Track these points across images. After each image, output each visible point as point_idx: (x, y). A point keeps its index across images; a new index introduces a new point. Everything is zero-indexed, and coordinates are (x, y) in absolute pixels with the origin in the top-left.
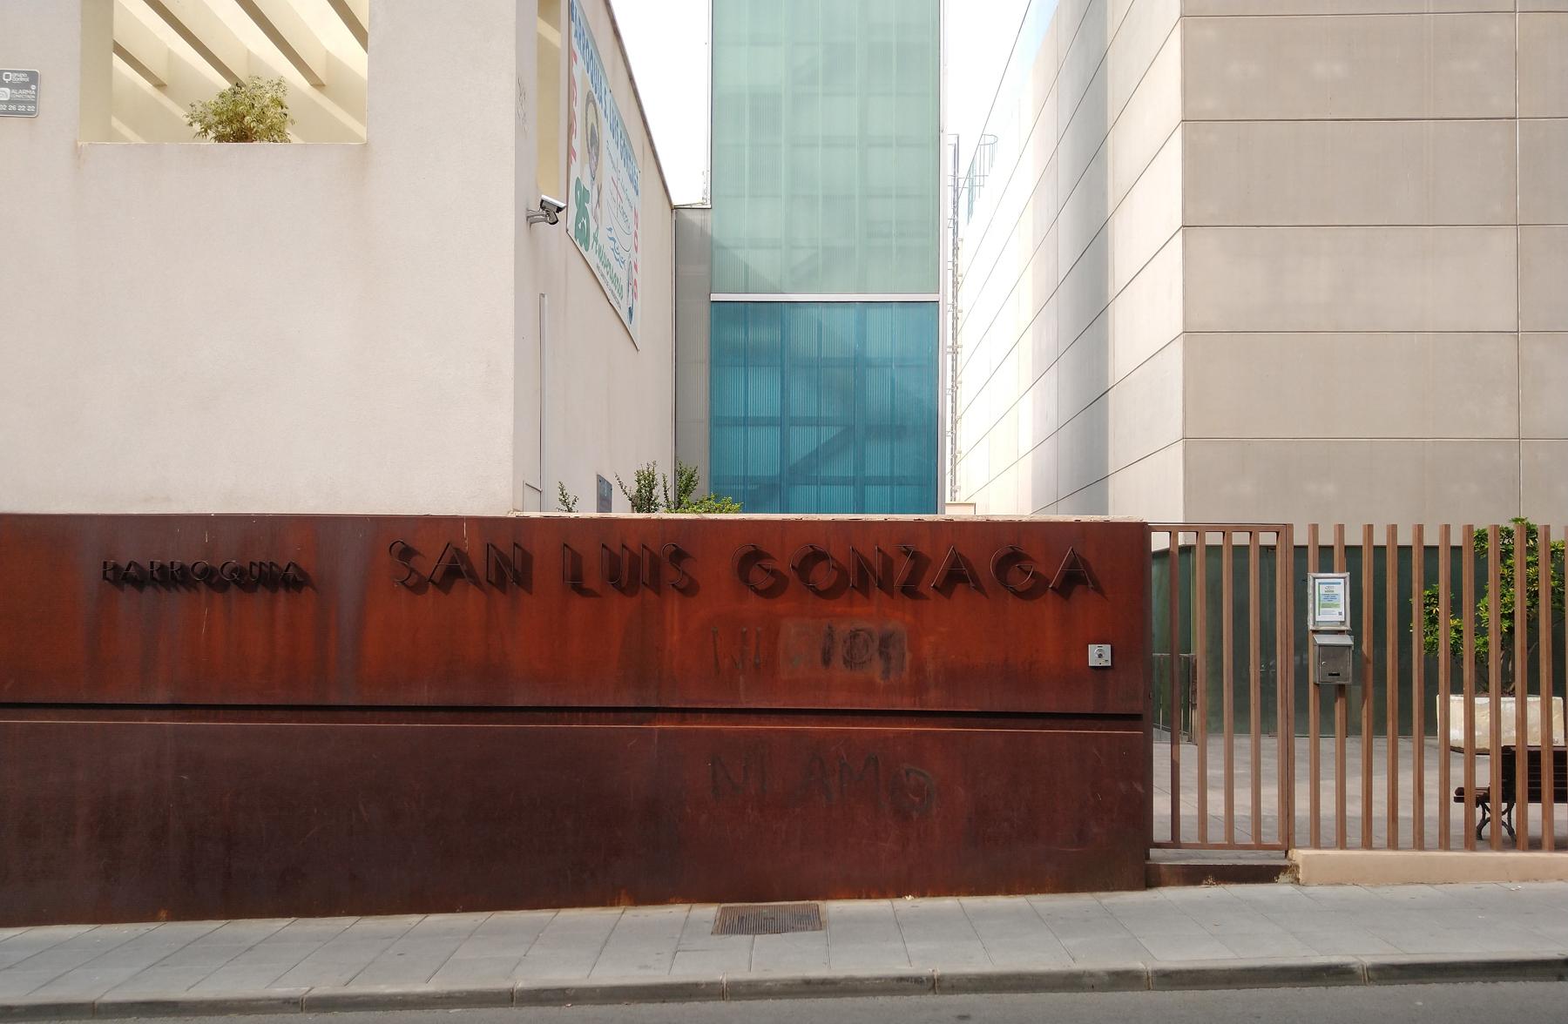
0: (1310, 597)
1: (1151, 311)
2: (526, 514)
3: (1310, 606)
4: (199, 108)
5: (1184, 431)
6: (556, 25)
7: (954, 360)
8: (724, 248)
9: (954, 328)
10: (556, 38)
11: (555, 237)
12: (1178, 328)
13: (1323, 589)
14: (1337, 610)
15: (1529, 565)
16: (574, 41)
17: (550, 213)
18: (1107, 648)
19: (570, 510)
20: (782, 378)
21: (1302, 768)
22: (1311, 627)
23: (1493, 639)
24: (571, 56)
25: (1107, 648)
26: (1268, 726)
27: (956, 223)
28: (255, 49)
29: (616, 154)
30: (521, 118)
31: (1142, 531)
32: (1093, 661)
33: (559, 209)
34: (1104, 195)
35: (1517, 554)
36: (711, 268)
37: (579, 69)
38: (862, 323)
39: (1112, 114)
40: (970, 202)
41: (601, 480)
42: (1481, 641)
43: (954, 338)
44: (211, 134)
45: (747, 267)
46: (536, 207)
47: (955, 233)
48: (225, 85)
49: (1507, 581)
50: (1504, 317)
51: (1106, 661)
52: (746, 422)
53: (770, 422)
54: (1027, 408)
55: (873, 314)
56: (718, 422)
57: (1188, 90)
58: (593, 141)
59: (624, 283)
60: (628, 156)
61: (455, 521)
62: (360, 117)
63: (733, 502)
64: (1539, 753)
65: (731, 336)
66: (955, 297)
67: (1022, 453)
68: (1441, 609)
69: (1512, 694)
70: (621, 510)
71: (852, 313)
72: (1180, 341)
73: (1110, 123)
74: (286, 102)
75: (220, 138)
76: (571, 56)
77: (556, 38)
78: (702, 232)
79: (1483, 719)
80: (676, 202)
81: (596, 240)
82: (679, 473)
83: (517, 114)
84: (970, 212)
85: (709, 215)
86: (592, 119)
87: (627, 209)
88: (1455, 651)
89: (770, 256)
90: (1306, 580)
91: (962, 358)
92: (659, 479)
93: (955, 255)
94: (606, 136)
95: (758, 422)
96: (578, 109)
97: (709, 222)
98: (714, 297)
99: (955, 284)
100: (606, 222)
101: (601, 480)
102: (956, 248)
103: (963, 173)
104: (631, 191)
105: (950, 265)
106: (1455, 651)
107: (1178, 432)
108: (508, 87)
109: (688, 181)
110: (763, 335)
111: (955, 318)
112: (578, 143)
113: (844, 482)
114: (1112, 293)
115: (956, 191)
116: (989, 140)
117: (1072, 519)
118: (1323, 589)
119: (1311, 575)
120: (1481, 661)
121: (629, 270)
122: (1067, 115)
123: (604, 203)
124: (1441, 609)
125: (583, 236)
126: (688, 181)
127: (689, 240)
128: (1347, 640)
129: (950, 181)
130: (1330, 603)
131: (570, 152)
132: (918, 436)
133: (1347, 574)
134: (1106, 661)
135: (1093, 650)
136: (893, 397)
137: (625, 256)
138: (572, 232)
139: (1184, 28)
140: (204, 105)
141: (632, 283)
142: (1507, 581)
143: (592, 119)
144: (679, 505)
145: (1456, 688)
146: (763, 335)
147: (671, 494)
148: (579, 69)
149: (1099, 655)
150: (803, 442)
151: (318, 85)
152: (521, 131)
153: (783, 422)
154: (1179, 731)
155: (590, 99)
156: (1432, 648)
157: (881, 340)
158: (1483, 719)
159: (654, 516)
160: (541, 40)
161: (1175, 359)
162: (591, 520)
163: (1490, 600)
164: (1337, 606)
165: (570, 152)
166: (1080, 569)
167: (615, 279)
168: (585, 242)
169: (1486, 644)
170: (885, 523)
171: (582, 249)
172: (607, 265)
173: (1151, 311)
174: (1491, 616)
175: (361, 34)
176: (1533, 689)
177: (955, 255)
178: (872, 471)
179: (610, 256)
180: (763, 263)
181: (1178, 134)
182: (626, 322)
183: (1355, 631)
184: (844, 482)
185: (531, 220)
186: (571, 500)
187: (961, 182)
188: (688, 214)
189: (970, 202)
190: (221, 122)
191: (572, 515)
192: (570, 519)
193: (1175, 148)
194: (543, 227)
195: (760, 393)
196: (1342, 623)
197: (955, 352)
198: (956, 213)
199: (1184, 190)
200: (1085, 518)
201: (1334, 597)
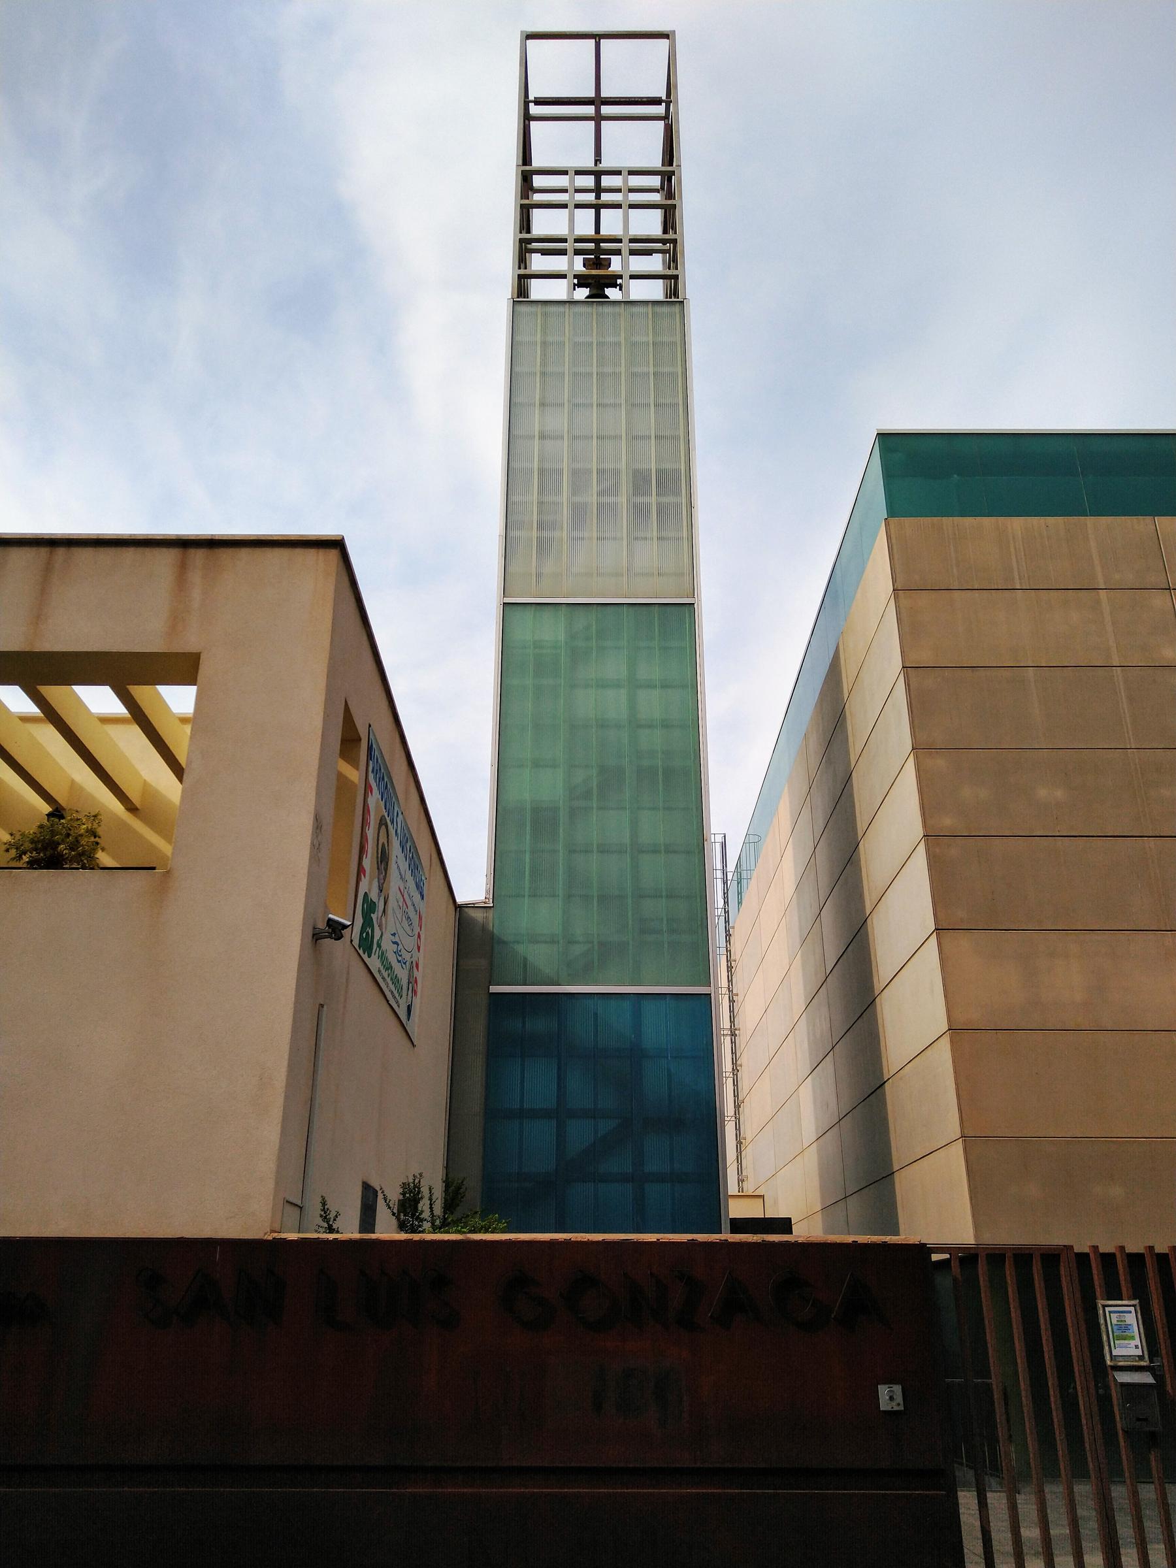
0: (1103, 1327)
1: (915, 1010)
2: (283, 1236)
3: (1105, 1338)
4: (18, 837)
6: (354, 763)
7: (733, 1042)
8: (504, 943)
9: (731, 1011)
10: (354, 775)
11: (340, 951)
13: (1114, 1318)
14: (1133, 1343)
16: (371, 776)
17: (336, 930)
18: (897, 1389)
19: (331, 1230)
20: (559, 1068)
21: (1125, 1531)
24: (368, 788)
25: (897, 1389)
26: (1079, 1472)
27: (727, 912)
28: (78, 778)
29: (404, 865)
30: (316, 848)
31: (922, 1250)
32: (885, 1404)
33: (345, 927)
34: (861, 896)
36: (491, 964)
37: (374, 799)
38: (637, 1015)
39: (861, 826)
40: (740, 893)
41: (366, 1187)
43: (732, 1022)
44: (25, 858)
45: (525, 959)
46: (322, 925)
47: (727, 921)
48: (46, 808)
51: (897, 1405)
52: (523, 1114)
53: (545, 1114)
54: (806, 1093)
55: (648, 1007)
56: (493, 1114)
58: (383, 858)
59: (404, 982)
60: (415, 865)
61: (209, 1244)
62: (168, 838)
63: (499, 1221)
65: (507, 1024)
66: (730, 981)
67: (806, 1145)
70: (387, 1230)
71: (627, 1004)
72: (946, 1038)
73: (860, 834)
74: (100, 831)
75: (33, 865)
76: (368, 788)
77: (354, 775)
78: (484, 928)
80: (460, 899)
81: (379, 946)
82: (447, 1183)
83: (313, 844)
84: (740, 903)
85: (491, 914)
86: (383, 839)
87: (412, 914)
89: (550, 953)
90: (1095, 1308)
91: (741, 1040)
92: (425, 1191)
93: (728, 941)
94: (396, 851)
95: (534, 1114)
96: (371, 833)
97: (492, 921)
98: (494, 989)
99: (730, 968)
100: (391, 929)
101: (366, 1187)
102: (728, 935)
103: (731, 867)
104: (417, 896)
105: (723, 951)
107: (951, 1125)
108: (305, 822)
109: (471, 882)
110: (540, 1025)
111: (732, 1001)
112: (367, 863)
114: (879, 983)
115: (725, 882)
116: (752, 839)
117: (849, 1239)
119: (1100, 1303)
121: (411, 969)
122: (821, 823)
123: (389, 911)
125: (367, 944)
126: (471, 882)
127: (472, 936)
128: (1147, 1378)
129: (719, 874)
131: (361, 870)
132: (693, 1125)
133: (1136, 1302)
134: (897, 1405)
135: (883, 1391)
137: (407, 956)
138: (356, 943)
139: (917, 758)
140: (23, 835)
141: (413, 981)
143: (383, 839)
144: (444, 1226)
146: (540, 1025)
147: (438, 1210)
148: (374, 799)
149: (889, 1397)
150: (580, 1134)
151: (132, 808)
152: (315, 858)
153: (560, 1114)
154: (987, 1469)
155: (382, 823)
157: (657, 1031)
159: (416, 1237)
160: (340, 777)
161: (943, 1054)
162: (351, 1242)
164: (1133, 1338)
165: (361, 870)
166: (859, 1292)
167: (396, 980)
168: (369, 950)
170: (658, 1243)
171: (365, 957)
172: (389, 967)
175: (178, 770)
177: (728, 941)
179: (392, 958)
180: (540, 956)
181: (922, 848)
182: (403, 1017)
185: (317, 936)
186: (332, 1215)
187: (730, 877)
188: (395, 1211)
189: (740, 893)
190: (36, 849)
191: (331, 1237)
192: (327, 1241)
193: (920, 860)
194: (327, 942)
195: (536, 1083)
196: (1141, 1358)
197: (733, 1035)
198: (726, 902)
200: (863, 1239)
201: (1127, 1327)
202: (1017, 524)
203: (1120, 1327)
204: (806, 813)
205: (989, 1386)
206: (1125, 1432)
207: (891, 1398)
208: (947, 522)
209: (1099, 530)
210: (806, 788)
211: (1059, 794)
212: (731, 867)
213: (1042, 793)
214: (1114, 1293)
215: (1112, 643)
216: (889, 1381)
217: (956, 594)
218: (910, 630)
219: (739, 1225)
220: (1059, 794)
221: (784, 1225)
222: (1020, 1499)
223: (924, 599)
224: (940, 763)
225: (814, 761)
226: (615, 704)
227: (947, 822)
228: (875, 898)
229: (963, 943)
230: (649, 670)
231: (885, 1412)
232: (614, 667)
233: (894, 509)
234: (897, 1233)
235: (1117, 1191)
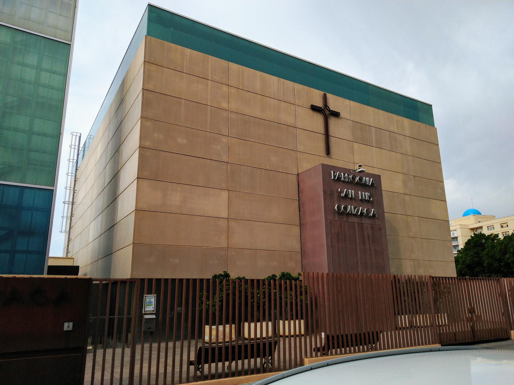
1: (127, 203)
5: (133, 241)
7: (72, 207)
12: (134, 209)
13: (148, 300)
14: (152, 307)
15: (227, 285)
18: (71, 324)
22: (143, 313)
23: (217, 308)
25: (71, 324)
27: (77, 161)
31: (90, 280)
35: (224, 282)
42: (214, 308)
49: (221, 290)
50: (225, 214)
51: (71, 328)
57: (142, 138)
64: (208, 348)
68: (204, 299)
69: (222, 324)
71: (18, 190)
72: (134, 213)
79: (214, 333)
88: (207, 311)
90: (143, 297)
103: (82, 145)
106: (207, 311)
107: (131, 240)
113: (6, 251)
118: (148, 300)
120: (214, 314)
124: (204, 299)
130: (150, 303)
132: (44, 234)
133: (155, 295)
134: (71, 328)
135: (66, 325)
136: (31, 221)
139: (141, 121)
142: (221, 290)
145: (207, 324)
149: (68, 326)
156: (201, 311)
157: (28, 200)
158: (214, 333)
163: (217, 296)
164: (152, 305)
169: (216, 309)
173: (127, 203)
174: (217, 300)
176: (227, 323)
178: (19, 248)
181: (138, 151)
183: (157, 314)
184: (6, 251)
187: (80, 149)
196: (153, 311)
199: (138, 167)
202: (188, 51)
203: (149, 302)
204: (107, 131)
205: (123, 318)
206: (144, 332)
207: (68, 327)
208: (166, 43)
209: (213, 61)
210: (108, 123)
211: (184, 141)
212: (82, 145)
213: (179, 140)
214: (150, 292)
215: (209, 98)
216: (68, 321)
217: (165, 69)
218: (147, 77)
219: (53, 270)
220: (184, 141)
221: (75, 270)
222: (169, 343)
223: (153, 68)
224: (149, 124)
225: (113, 113)
226: (30, 74)
227: (148, 144)
228: (123, 164)
229: (145, 183)
230: (46, 64)
231: (66, 331)
232: (32, 59)
233: (149, 33)
234: (78, 275)
235: (177, 261)
